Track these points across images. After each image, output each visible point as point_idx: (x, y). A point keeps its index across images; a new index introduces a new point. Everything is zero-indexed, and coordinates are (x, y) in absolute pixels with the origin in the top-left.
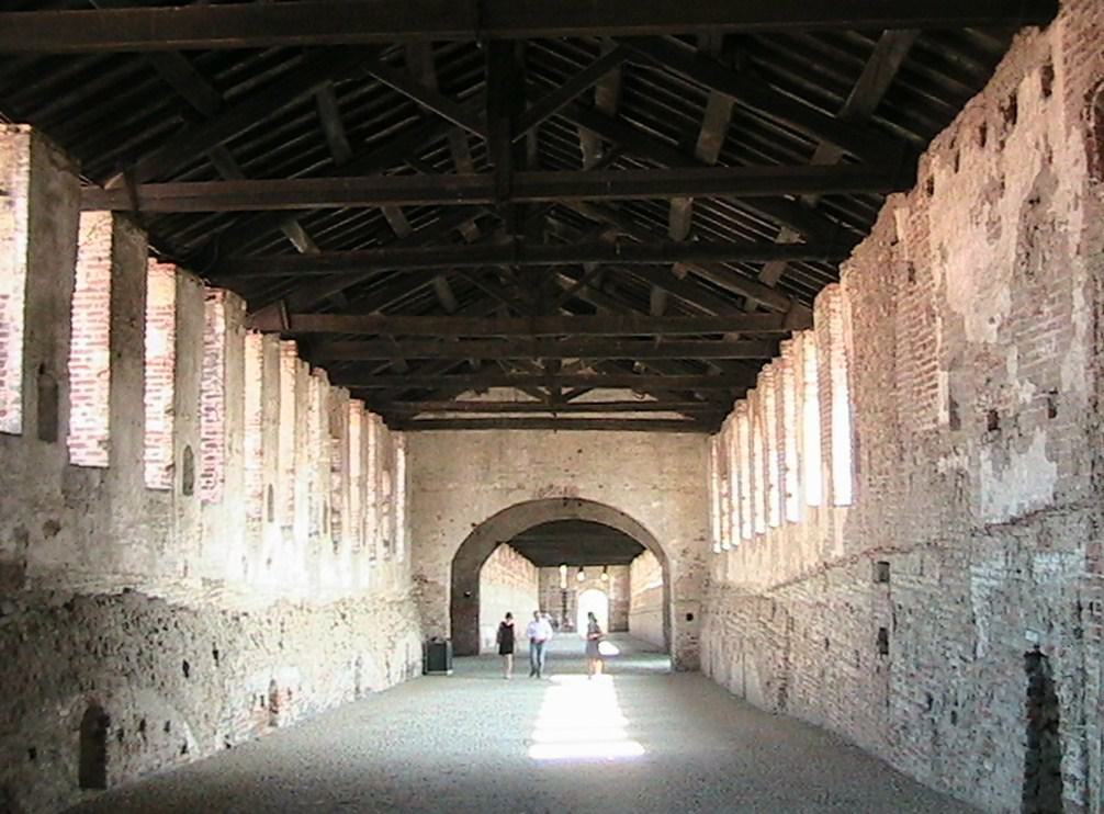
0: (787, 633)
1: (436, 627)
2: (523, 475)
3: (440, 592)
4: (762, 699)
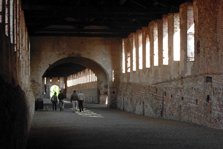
0: (163, 96)
1: (38, 96)
2: (65, 50)
3: (39, 85)
4: (154, 115)
